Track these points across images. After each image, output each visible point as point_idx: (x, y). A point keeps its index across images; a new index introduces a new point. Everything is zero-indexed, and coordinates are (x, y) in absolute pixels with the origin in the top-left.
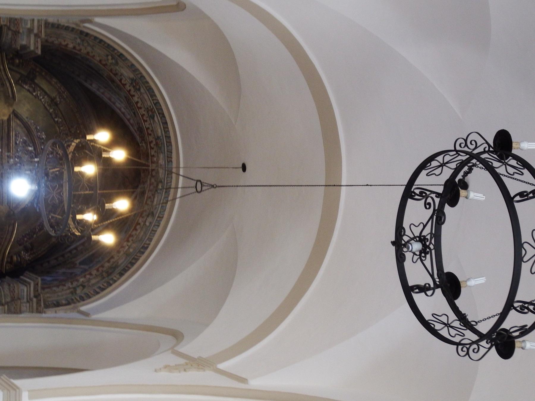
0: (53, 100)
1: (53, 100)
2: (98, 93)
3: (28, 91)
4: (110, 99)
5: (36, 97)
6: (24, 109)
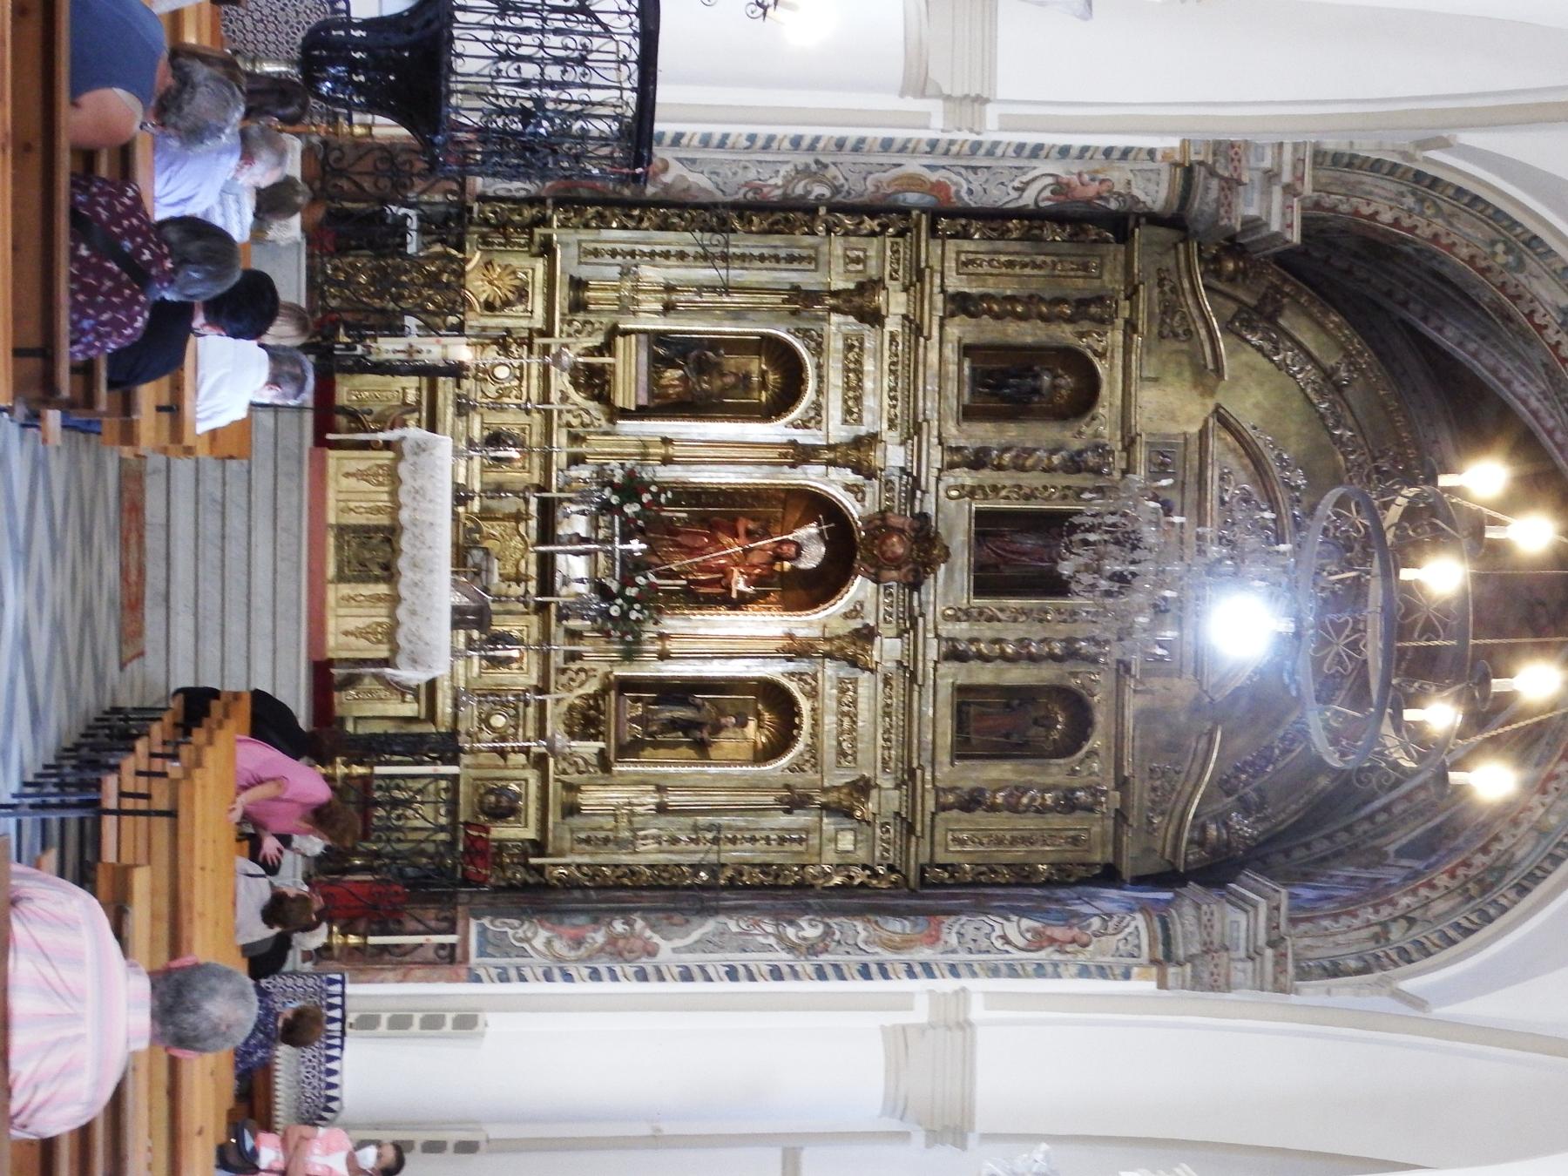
0: (1328, 375)
1: (1328, 375)
2: (1461, 354)
3: (1259, 349)
4: (1494, 372)
5: (1279, 366)
6: (1249, 402)
